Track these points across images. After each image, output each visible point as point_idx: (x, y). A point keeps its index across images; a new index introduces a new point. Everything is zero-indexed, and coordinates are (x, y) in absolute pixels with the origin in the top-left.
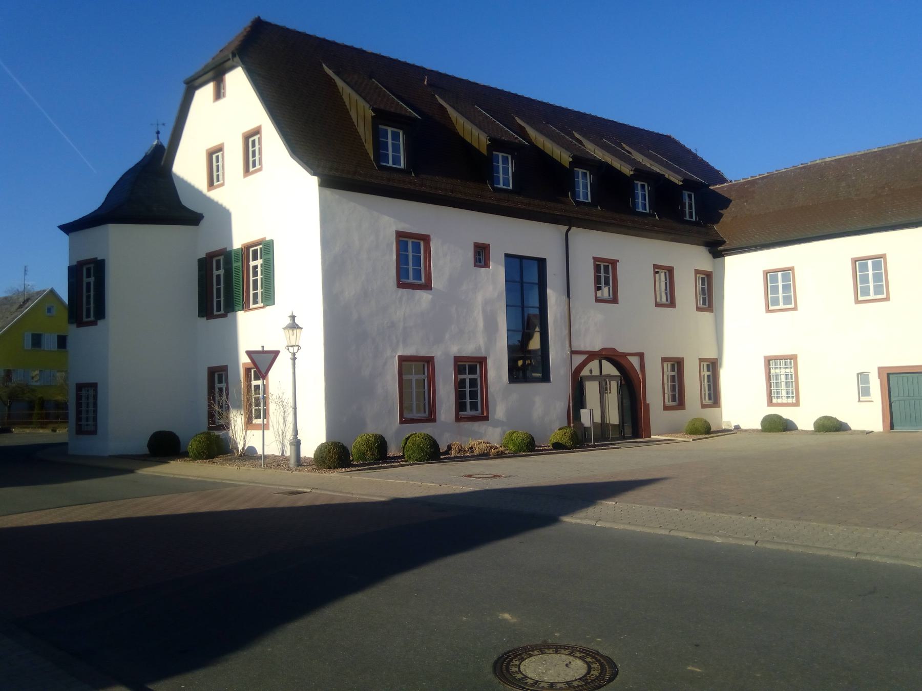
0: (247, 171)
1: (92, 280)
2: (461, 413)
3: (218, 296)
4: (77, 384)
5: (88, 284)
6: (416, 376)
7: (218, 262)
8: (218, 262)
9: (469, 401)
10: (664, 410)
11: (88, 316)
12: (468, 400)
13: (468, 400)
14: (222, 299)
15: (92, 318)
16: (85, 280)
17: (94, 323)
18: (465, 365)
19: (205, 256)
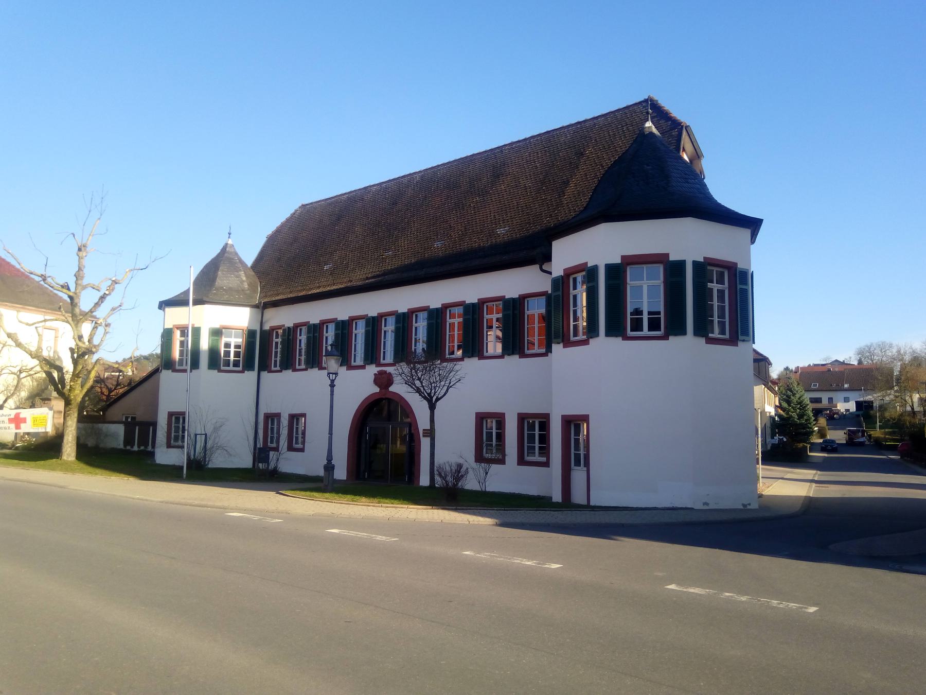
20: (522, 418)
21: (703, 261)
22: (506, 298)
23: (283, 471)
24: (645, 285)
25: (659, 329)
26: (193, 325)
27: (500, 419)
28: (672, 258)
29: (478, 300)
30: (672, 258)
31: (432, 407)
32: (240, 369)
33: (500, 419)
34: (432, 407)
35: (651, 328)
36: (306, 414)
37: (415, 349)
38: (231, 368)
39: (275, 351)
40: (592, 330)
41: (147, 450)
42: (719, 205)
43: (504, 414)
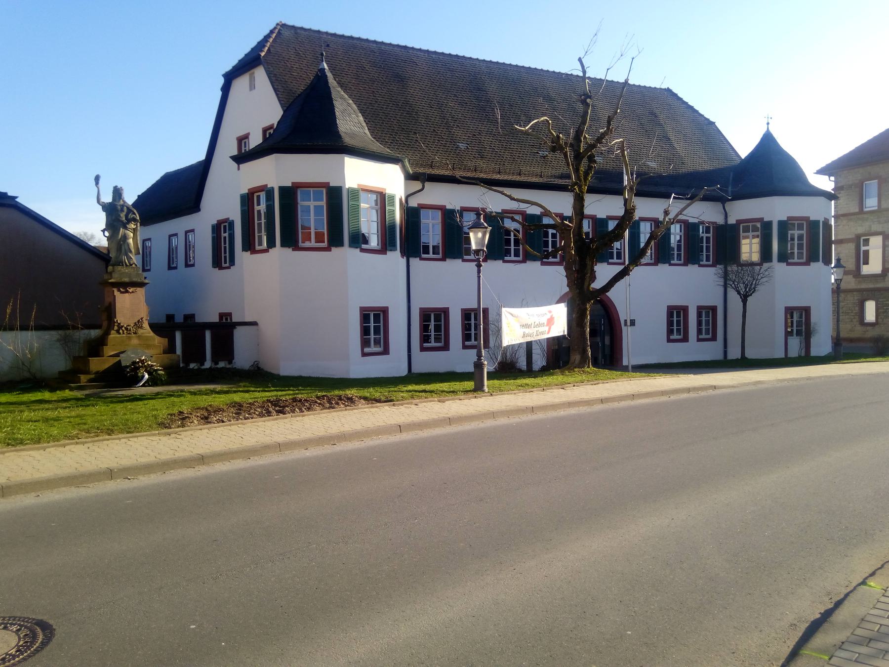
0: (251, 89)
1: (227, 235)
2: (424, 344)
3: (225, 253)
4: (184, 315)
5: (259, 204)
6: (798, 231)
7: (225, 227)
8: (225, 227)
9: (373, 325)
10: (697, 341)
11: (225, 263)
12: (675, 328)
13: (675, 328)
14: (223, 255)
15: (227, 265)
16: (223, 235)
17: (228, 268)
18: (433, 254)
19: (247, 192)
20: (700, 309)
21: (291, 185)
22: (268, 187)
23: (811, 339)
24: (312, 204)
25: (519, 256)
26: (832, 190)
27: (685, 310)
28: (765, 220)
29: (292, 183)
30: (765, 220)
31: (744, 302)
32: (520, 258)
33: (685, 310)
34: (744, 302)
35: (515, 256)
36: (194, 315)
37: (87, 237)
38: (431, 255)
39: (258, 223)
40: (271, 244)
41: (203, 367)
42: (813, 187)
43: (688, 306)
